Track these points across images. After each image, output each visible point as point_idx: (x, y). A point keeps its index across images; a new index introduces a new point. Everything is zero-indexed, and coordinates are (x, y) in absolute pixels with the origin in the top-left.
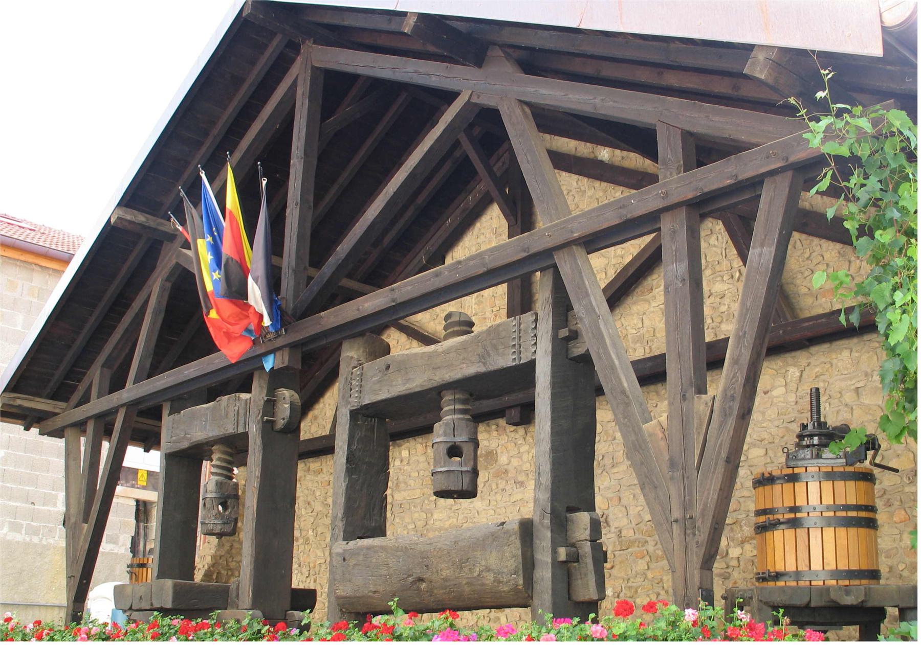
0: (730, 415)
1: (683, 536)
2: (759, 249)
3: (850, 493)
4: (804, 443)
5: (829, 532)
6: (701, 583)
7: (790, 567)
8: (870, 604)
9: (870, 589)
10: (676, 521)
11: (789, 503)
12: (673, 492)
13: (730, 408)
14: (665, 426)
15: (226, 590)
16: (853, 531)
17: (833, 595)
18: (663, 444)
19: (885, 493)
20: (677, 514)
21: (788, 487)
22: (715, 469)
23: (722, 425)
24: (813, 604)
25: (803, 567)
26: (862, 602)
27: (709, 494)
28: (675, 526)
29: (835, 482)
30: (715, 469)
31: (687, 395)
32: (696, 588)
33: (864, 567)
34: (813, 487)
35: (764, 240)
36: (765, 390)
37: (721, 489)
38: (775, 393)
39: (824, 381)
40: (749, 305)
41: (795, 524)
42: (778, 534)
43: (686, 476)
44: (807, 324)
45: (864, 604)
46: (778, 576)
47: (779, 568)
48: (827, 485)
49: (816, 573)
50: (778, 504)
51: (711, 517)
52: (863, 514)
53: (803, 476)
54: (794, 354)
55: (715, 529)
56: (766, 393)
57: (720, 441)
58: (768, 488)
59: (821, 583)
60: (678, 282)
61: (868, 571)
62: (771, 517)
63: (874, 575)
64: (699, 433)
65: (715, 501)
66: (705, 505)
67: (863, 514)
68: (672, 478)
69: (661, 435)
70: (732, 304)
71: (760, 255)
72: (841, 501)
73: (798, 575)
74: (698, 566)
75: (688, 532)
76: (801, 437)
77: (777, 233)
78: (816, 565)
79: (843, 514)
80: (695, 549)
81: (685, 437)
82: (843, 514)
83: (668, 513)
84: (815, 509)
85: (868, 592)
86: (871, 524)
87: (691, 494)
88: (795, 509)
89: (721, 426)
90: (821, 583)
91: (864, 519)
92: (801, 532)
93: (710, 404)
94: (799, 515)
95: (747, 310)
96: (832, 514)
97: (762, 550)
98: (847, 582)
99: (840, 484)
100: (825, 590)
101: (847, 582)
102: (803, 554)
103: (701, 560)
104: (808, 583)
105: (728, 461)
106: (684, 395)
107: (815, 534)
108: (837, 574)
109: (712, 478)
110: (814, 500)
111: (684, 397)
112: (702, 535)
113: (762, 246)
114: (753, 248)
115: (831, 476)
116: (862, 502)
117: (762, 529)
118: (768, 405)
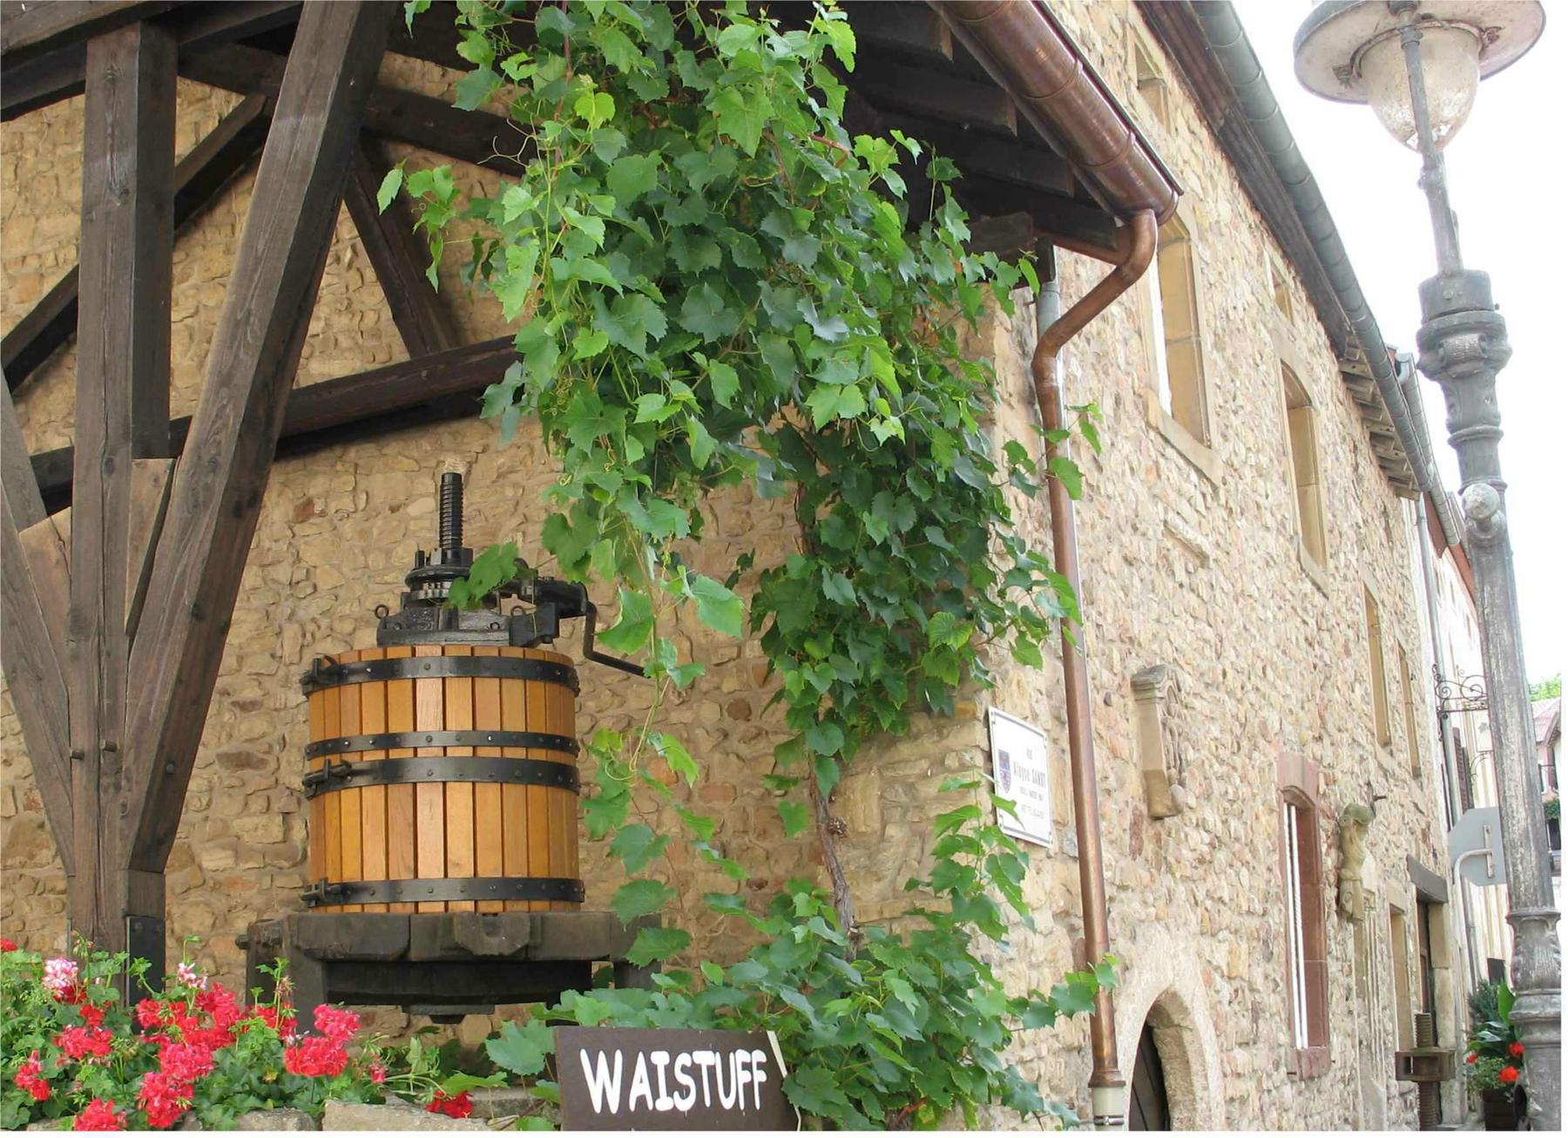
0: (206, 506)
1: (93, 792)
2: (292, 120)
3: (511, 706)
4: (422, 595)
5: (460, 794)
6: (129, 902)
7: (374, 872)
8: (542, 955)
9: (544, 919)
10: (79, 756)
11: (374, 727)
12: (78, 689)
13: (207, 488)
14: (66, 534)
15: (1522, 1097)
16: (514, 792)
17: (459, 936)
18: (59, 575)
19: (629, 725)
20: (82, 740)
21: (372, 690)
22: (168, 633)
23: (187, 527)
24: (414, 955)
25: (400, 873)
26: (526, 947)
27: (152, 691)
28: (78, 769)
29: (478, 681)
30: (168, 633)
31: (117, 459)
32: (120, 914)
33: (539, 872)
34: (428, 690)
35: (304, 99)
36: (395, 503)
37: (179, 680)
38: (413, 510)
39: (515, 485)
40: (260, 247)
41: (389, 773)
42: (348, 797)
43: (104, 649)
44: (476, 359)
45: (531, 954)
46: (346, 892)
47: (350, 874)
48: (460, 688)
49: (431, 887)
50: (350, 730)
51: (155, 748)
52: (539, 755)
53: (407, 665)
54: (455, 426)
55: (168, 775)
56: (393, 510)
57: (183, 565)
58: (331, 693)
59: (440, 908)
60: (114, 198)
61: (548, 881)
62: (335, 760)
63: (567, 890)
64: (136, 549)
65: (164, 709)
66: (144, 719)
67: (539, 755)
68: (75, 657)
69: (55, 555)
70: (335, 318)
71: (295, 131)
72: (489, 724)
73: (393, 889)
74: (125, 862)
75: (105, 781)
76: (415, 581)
77: (335, 81)
78: (430, 867)
79: (495, 752)
80: (118, 823)
81: (108, 560)
82: (495, 752)
83: (64, 740)
84: (429, 739)
85: (538, 925)
86: (562, 777)
87: (114, 694)
88: (388, 740)
89: (184, 532)
90: (440, 908)
91: (548, 764)
92: (399, 792)
93: (164, 480)
94: (395, 754)
95: (258, 261)
96: (468, 752)
97: (317, 834)
98: (497, 906)
99: (488, 687)
100: (446, 921)
101: (497, 906)
102: (401, 846)
103: (130, 848)
104: (410, 908)
105: (197, 613)
106: (110, 461)
107: (429, 797)
108: (476, 887)
109: (161, 654)
110: (428, 720)
111: (109, 466)
112: (135, 791)
113: (300, 112)
114: (279, 118)
115: (470, 667)
116: (538, 727)
117: (319, 786)
118: (399, 535)
